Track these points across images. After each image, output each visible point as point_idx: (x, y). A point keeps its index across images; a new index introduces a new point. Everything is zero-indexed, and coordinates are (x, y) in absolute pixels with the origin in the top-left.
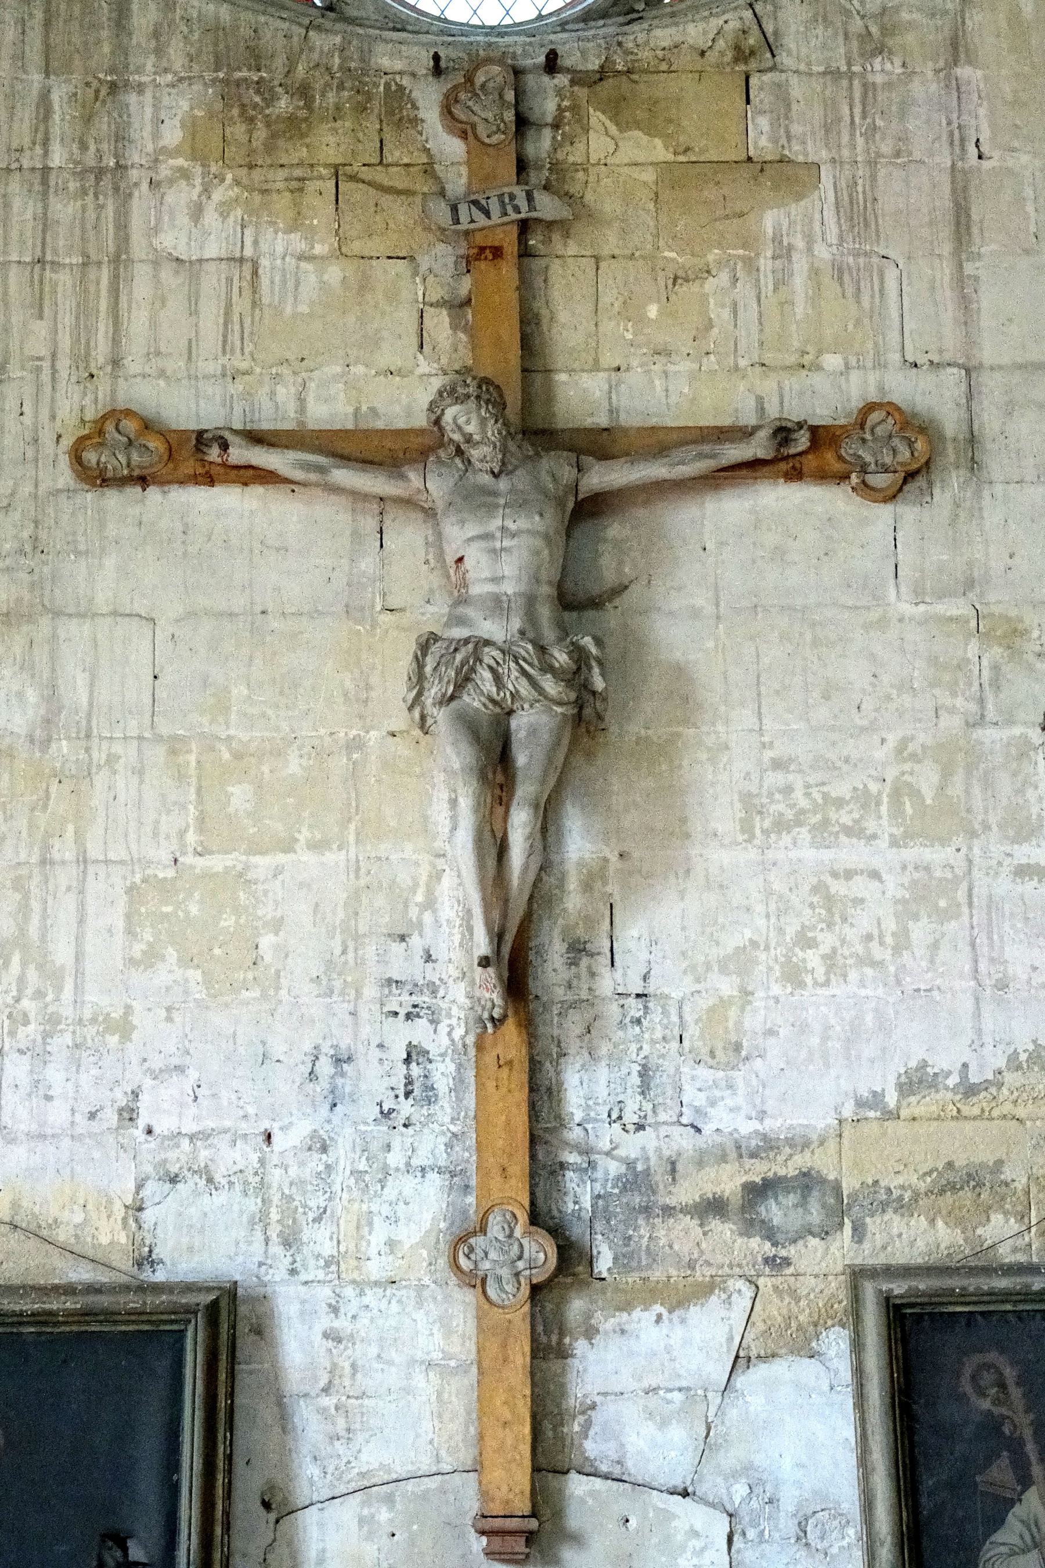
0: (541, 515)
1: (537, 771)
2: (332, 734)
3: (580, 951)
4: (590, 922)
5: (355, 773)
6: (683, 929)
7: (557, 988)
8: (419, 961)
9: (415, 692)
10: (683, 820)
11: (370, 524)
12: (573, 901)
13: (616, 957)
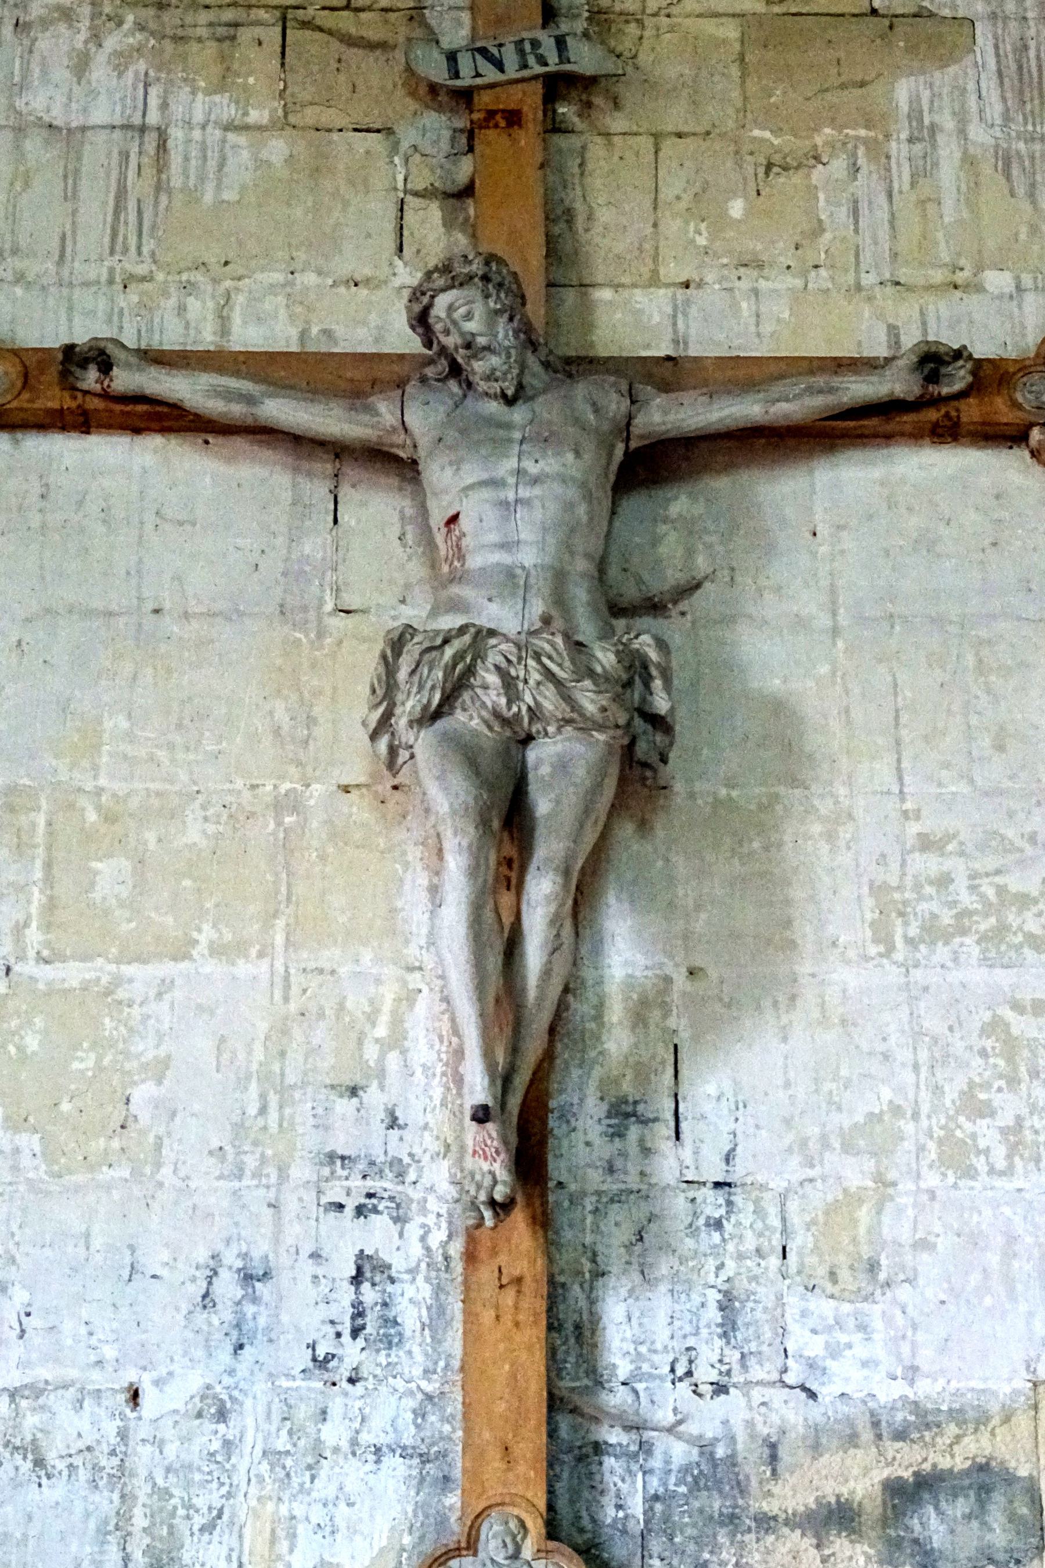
1: (569, 814)
2: (254, 787)
3: (627, 1115)
4: (643, 1073)
6: (787, 1085)
8: (378, 1127)
9: (381, 710)
10: (788, 923)
13: (683, 1125)
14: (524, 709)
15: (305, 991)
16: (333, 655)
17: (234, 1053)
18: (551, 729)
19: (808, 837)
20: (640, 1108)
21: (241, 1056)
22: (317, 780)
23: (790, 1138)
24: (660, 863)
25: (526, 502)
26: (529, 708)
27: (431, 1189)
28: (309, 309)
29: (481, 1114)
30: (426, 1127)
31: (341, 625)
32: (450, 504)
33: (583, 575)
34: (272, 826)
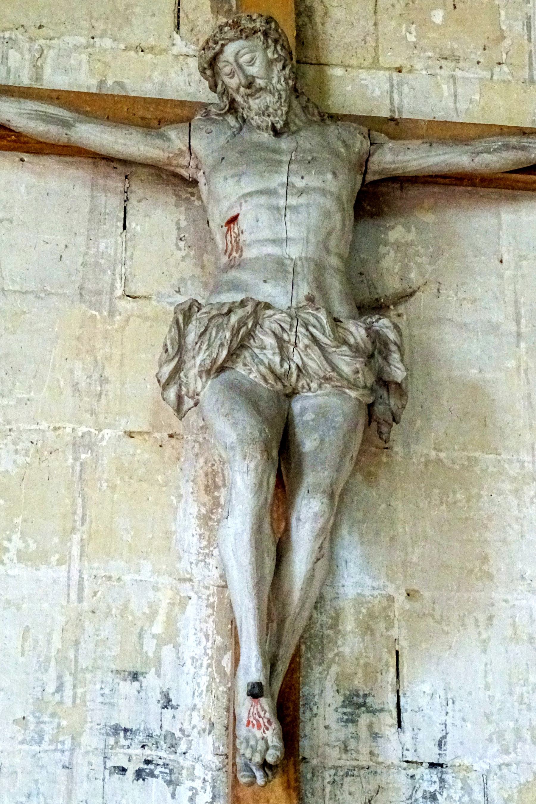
0: (334, 174)
1: (331, 452)
2: (55, 429)
3: (359, 706)
4: (371, 673)
5: (82, 476)
6: (487, 687)
7: (328, 750)
8: (155, 708)
9: (173, 364)
10: (485, 559)
11: (114, 203)
12: (350, 644)
13: (404, 715)
14: (293, 366)
15: (95, 594)
16: (123, 329)
17: (36, 641)
18: (314, 385)
19: (500, 492)
20: (369, 700)
21: (42, 643)
22: (109, 426)
23: (491, 728)
24: (384, 506)
25: (295, 209)
26: (298, 366)
27: (198, 759)
28: (107, 65)
29: (256, 691)
30: (194, 708)
31: (129, 307)
32: (231, 207)
33: (337, 270)
34: (70, 461)
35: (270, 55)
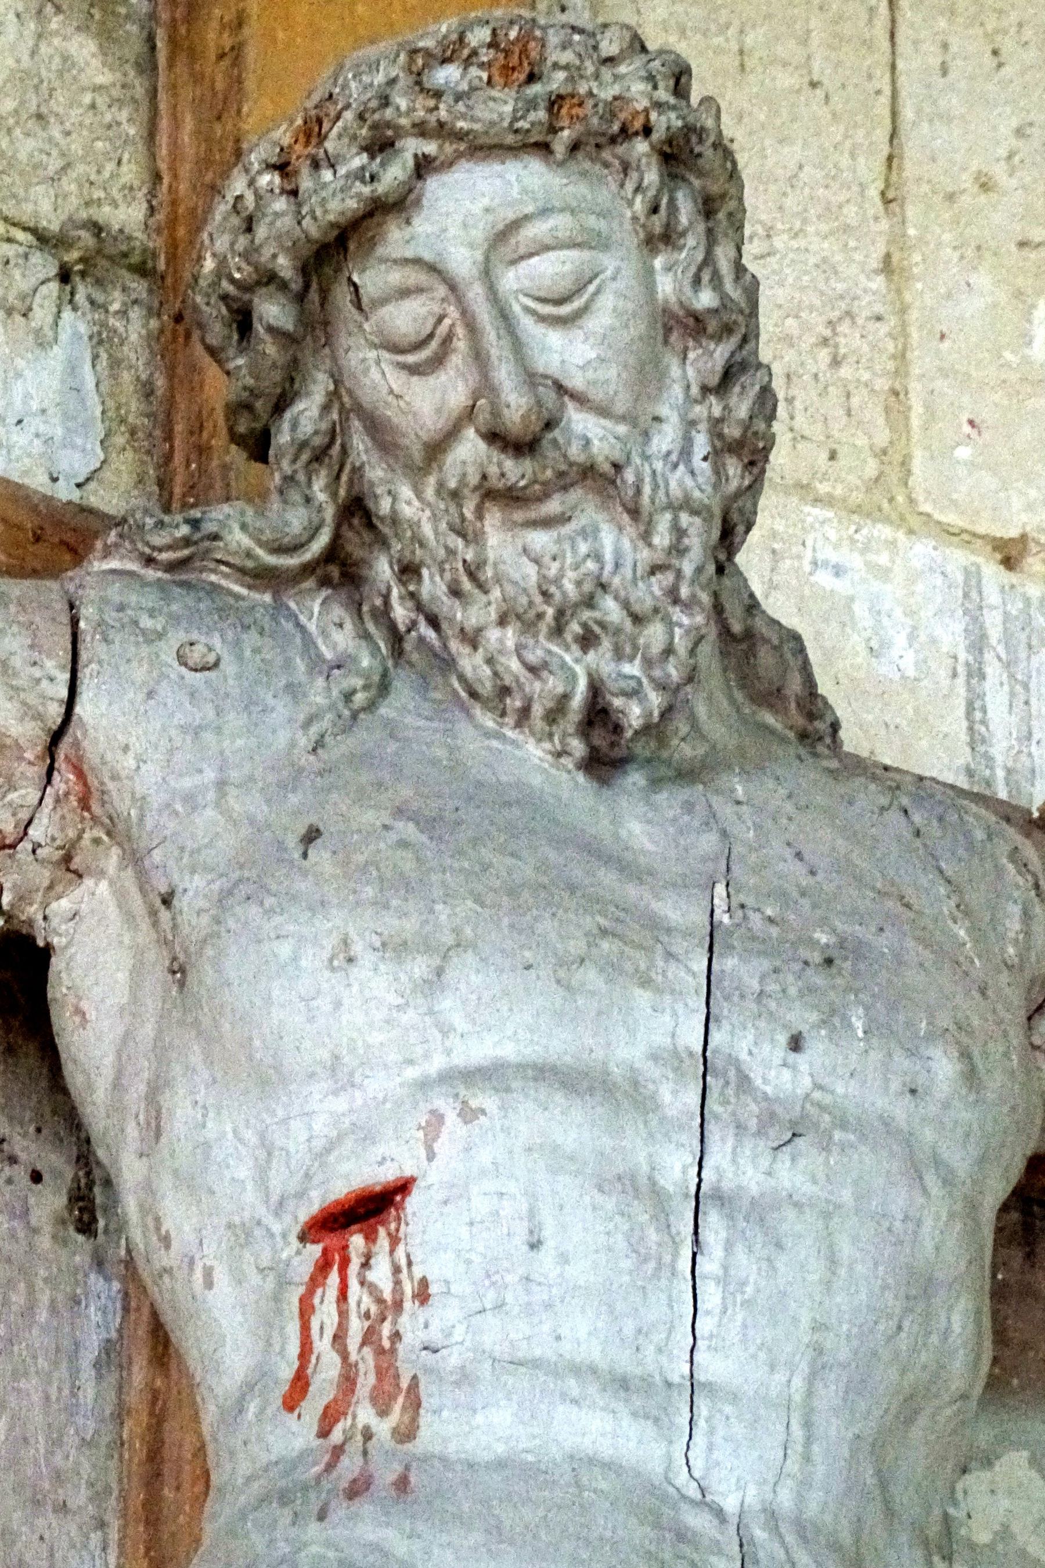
25: (757, 1214)
35: (666, 286)
